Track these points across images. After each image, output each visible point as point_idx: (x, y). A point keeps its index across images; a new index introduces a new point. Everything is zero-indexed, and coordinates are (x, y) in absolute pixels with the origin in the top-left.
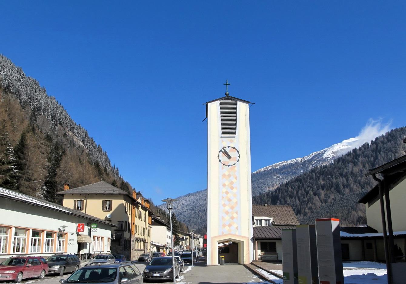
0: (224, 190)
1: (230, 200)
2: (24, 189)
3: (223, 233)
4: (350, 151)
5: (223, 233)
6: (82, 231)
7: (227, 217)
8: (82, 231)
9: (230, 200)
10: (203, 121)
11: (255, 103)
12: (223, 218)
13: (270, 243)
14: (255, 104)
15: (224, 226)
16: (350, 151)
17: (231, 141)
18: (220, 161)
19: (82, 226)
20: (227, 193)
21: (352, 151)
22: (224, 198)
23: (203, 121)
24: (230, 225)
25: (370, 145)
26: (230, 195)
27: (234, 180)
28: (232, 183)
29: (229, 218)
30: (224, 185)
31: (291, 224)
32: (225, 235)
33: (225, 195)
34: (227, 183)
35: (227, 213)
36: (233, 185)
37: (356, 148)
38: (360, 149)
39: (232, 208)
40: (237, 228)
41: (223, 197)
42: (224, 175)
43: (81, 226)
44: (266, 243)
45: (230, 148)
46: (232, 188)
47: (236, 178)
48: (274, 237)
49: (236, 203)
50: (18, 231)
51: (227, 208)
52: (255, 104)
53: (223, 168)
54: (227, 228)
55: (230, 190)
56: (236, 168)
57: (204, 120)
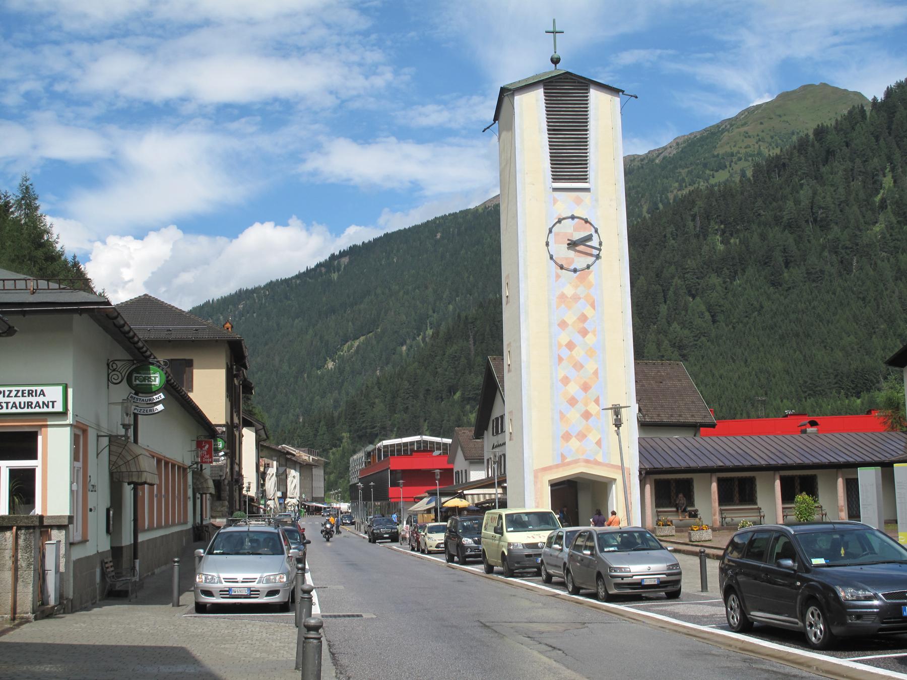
0: (564, 338)
1: (578, 366)
2: (849, 493)
3: (563, 457)
4: (807, 135)
5: (563, 457)
6: (208, 460)
7: (574, 415)
8: (208, 460)
9: (578, 366)
10: (483, 131)
11: (638, 96)
12: (562, 416)
13: (678, 481)
14: (636, 97)
15: (567, 437)
16: (807, 135)
17: (579, 202)
18: (551, 258)
19: (207, 446)
20: (571, 346)
21: (812, 136)
22: (563, 359)
23: (483, 131)
24: (582, 436)
25: (868, 114)
26: (579, 353)
27: (589, 312)
28: (583, 318)
29: (578, 415)
30: (563, 325)
31: (691, 420)
32: (569, 464)
33: (565, 352)
34: (571, 318)
35: (573, 402)
36: (586, 325)
37: (825, 124)
38: (838, 128)
39: (586, 387)
40: (599, 443)
41: (560, 359)
42: (563, 297)
43: (204, 446)
44: (668, 482)
45: (576, 220)
46: (584, 333)
47: (593, 306)
48: (691, 465)
49: (596, 373)
50: (723, 512)
51: (573, 389)
52: (636, 97)
53: (558, 276)
54: (574, 443)
55: (578, 339)
56: (592, 277)
57: (488, 128)
